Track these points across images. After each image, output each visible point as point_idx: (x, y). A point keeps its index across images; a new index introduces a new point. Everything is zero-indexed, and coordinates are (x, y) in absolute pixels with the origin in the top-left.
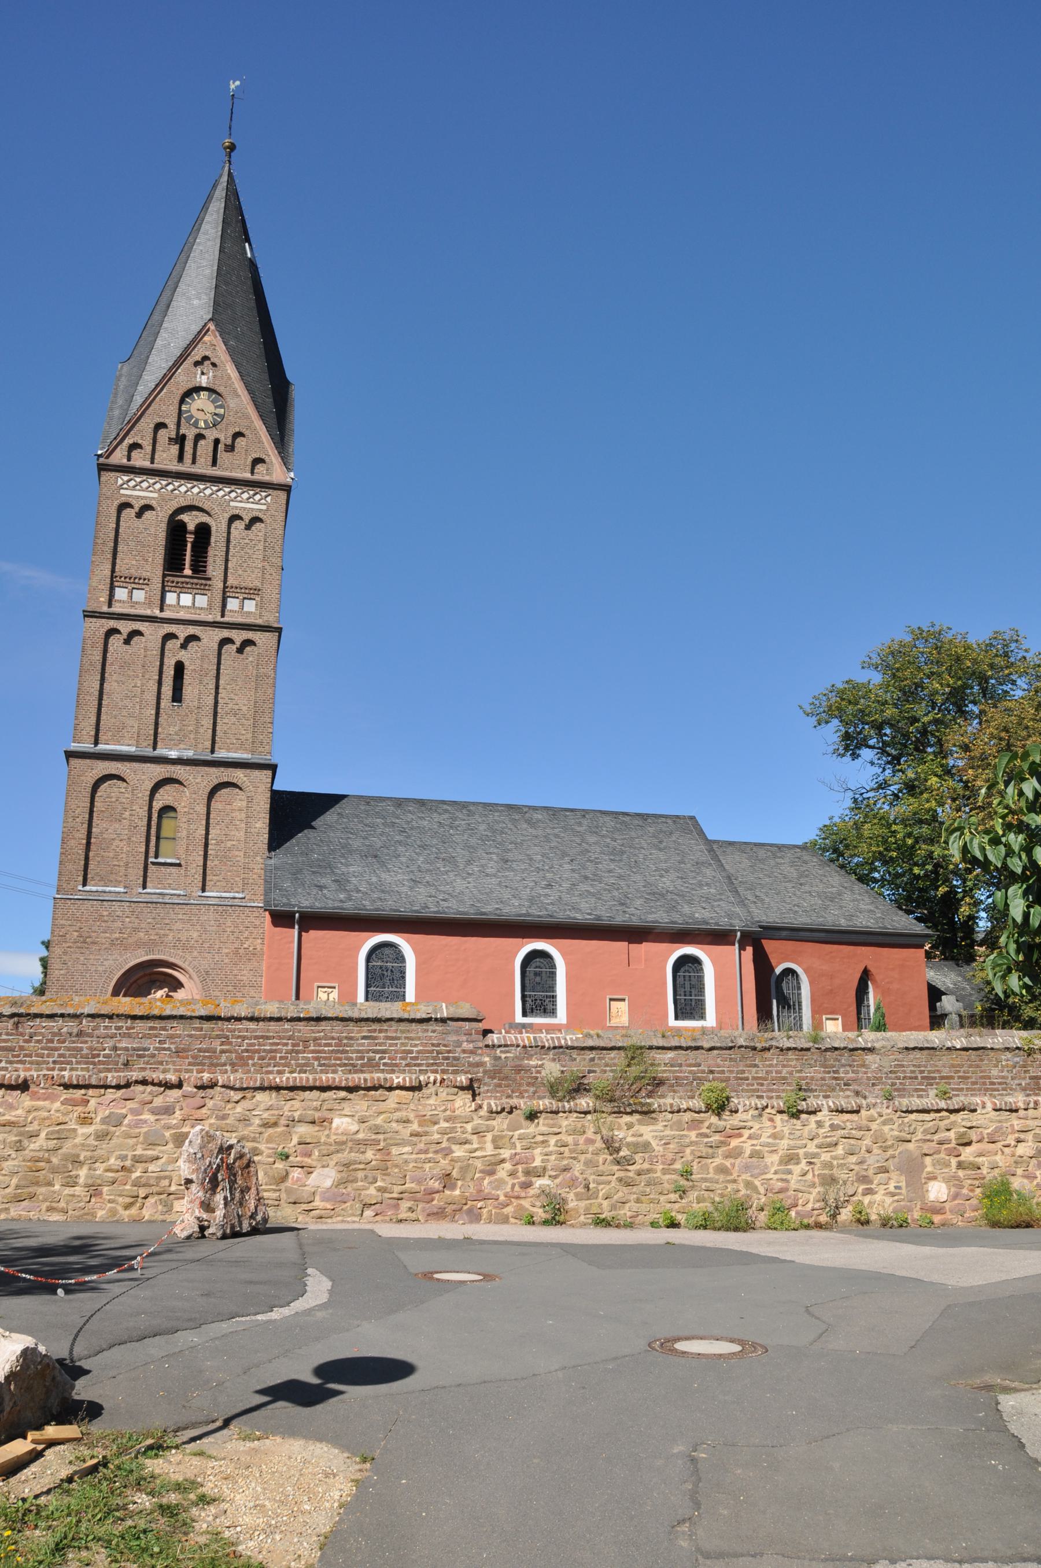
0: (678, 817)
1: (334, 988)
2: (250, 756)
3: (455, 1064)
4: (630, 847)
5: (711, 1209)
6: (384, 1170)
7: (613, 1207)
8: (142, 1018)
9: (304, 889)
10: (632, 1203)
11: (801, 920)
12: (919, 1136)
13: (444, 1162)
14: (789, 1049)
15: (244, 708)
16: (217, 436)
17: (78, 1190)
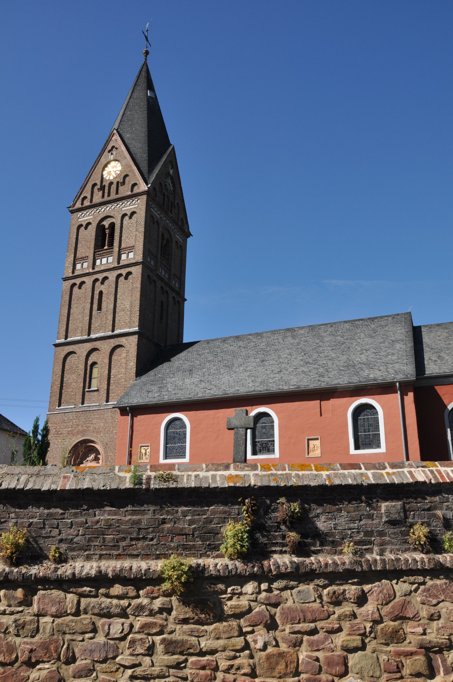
1: (148, 446)
15: (128, 306)
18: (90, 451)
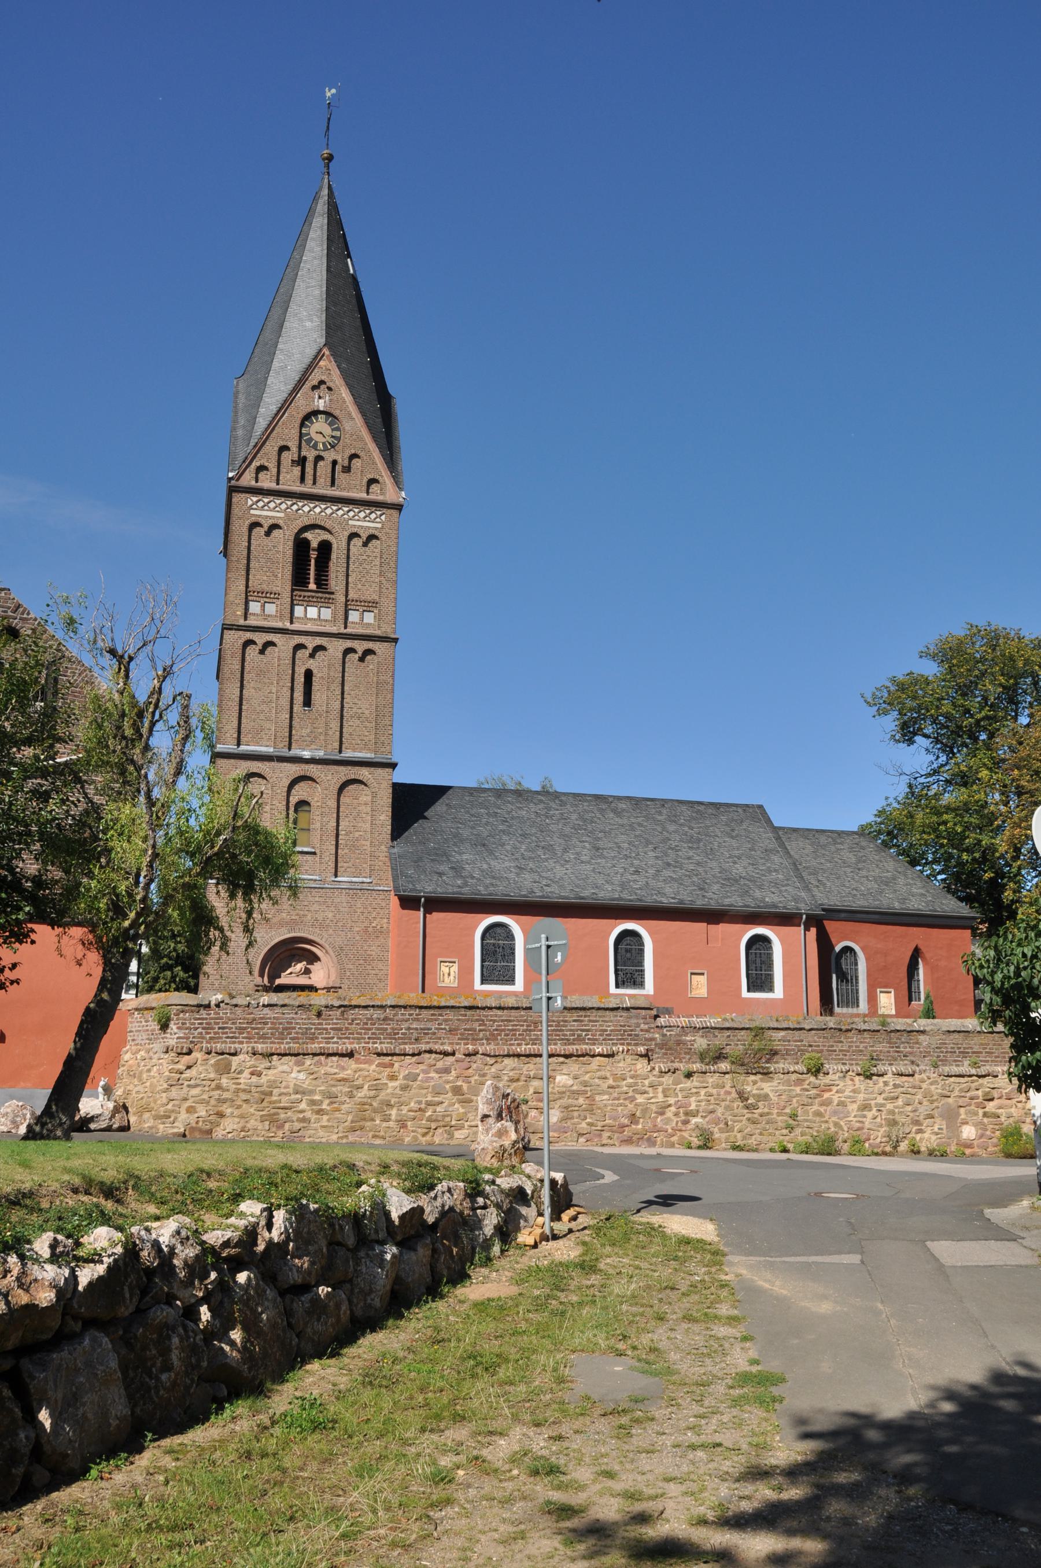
0: (747, 806)
2: (373, 756)
3: (636, 1040)
4: (706, 835)
5: (810, 1140)
6: (591, 1111)
7: (744, 1138)
8: (426, 1008)
9: (426, 876)
10: (757, 1136)
11: (860, 903)
12: (956, 1093)
13: (631, 1106)
14: (865, 1030)
15: (367, 712)
16: (335, 457)
17: (391, 1124)
18: (294, 956)
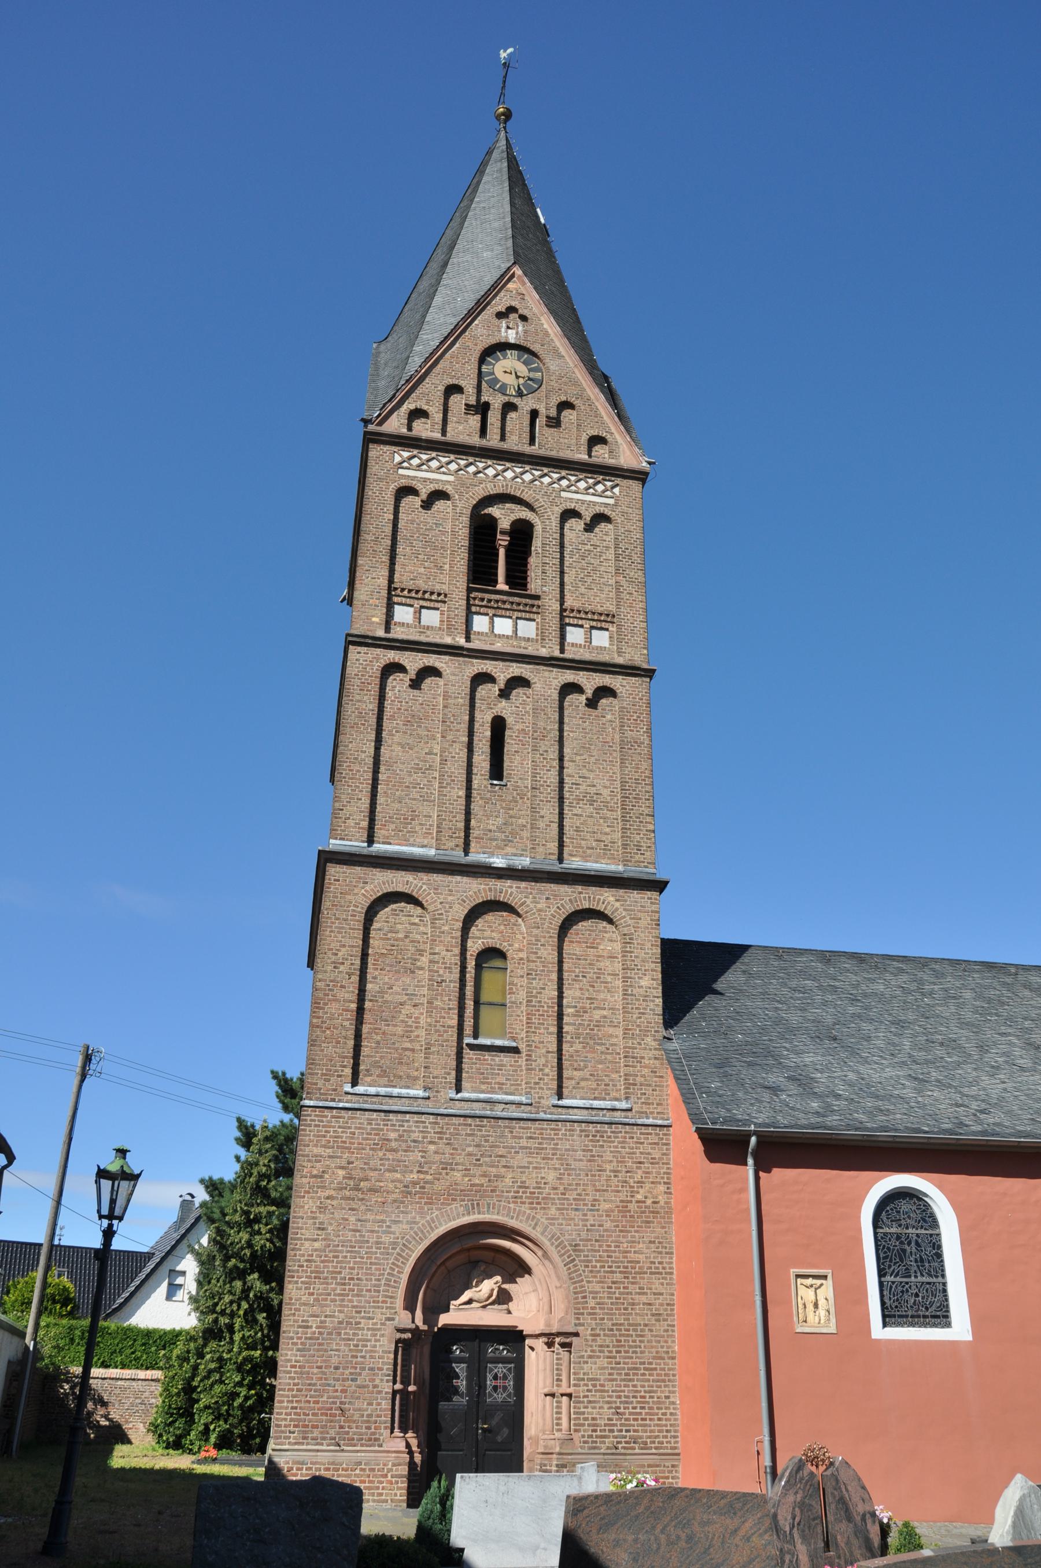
1: (825, 1277)
2: (621, 868)
15: (606, 792)
18: (474, 1264)
